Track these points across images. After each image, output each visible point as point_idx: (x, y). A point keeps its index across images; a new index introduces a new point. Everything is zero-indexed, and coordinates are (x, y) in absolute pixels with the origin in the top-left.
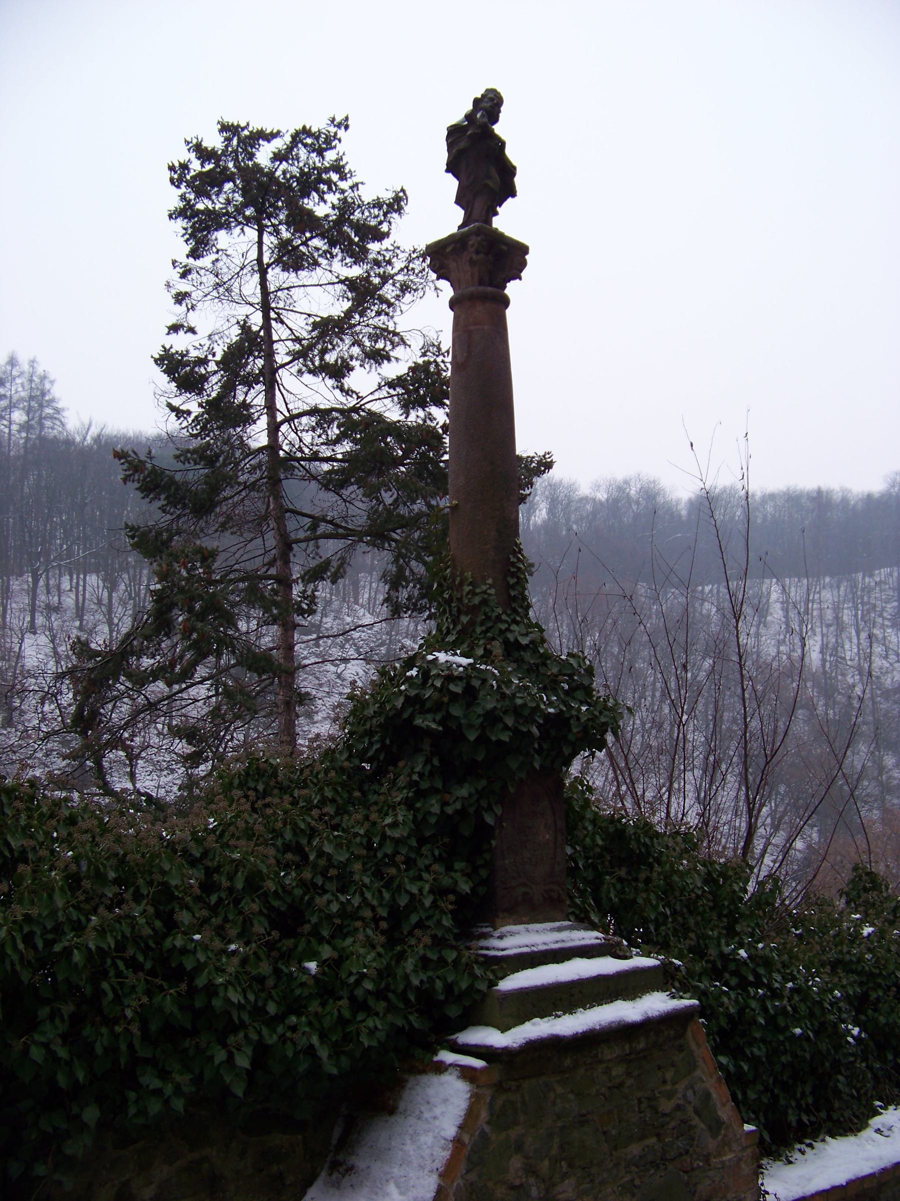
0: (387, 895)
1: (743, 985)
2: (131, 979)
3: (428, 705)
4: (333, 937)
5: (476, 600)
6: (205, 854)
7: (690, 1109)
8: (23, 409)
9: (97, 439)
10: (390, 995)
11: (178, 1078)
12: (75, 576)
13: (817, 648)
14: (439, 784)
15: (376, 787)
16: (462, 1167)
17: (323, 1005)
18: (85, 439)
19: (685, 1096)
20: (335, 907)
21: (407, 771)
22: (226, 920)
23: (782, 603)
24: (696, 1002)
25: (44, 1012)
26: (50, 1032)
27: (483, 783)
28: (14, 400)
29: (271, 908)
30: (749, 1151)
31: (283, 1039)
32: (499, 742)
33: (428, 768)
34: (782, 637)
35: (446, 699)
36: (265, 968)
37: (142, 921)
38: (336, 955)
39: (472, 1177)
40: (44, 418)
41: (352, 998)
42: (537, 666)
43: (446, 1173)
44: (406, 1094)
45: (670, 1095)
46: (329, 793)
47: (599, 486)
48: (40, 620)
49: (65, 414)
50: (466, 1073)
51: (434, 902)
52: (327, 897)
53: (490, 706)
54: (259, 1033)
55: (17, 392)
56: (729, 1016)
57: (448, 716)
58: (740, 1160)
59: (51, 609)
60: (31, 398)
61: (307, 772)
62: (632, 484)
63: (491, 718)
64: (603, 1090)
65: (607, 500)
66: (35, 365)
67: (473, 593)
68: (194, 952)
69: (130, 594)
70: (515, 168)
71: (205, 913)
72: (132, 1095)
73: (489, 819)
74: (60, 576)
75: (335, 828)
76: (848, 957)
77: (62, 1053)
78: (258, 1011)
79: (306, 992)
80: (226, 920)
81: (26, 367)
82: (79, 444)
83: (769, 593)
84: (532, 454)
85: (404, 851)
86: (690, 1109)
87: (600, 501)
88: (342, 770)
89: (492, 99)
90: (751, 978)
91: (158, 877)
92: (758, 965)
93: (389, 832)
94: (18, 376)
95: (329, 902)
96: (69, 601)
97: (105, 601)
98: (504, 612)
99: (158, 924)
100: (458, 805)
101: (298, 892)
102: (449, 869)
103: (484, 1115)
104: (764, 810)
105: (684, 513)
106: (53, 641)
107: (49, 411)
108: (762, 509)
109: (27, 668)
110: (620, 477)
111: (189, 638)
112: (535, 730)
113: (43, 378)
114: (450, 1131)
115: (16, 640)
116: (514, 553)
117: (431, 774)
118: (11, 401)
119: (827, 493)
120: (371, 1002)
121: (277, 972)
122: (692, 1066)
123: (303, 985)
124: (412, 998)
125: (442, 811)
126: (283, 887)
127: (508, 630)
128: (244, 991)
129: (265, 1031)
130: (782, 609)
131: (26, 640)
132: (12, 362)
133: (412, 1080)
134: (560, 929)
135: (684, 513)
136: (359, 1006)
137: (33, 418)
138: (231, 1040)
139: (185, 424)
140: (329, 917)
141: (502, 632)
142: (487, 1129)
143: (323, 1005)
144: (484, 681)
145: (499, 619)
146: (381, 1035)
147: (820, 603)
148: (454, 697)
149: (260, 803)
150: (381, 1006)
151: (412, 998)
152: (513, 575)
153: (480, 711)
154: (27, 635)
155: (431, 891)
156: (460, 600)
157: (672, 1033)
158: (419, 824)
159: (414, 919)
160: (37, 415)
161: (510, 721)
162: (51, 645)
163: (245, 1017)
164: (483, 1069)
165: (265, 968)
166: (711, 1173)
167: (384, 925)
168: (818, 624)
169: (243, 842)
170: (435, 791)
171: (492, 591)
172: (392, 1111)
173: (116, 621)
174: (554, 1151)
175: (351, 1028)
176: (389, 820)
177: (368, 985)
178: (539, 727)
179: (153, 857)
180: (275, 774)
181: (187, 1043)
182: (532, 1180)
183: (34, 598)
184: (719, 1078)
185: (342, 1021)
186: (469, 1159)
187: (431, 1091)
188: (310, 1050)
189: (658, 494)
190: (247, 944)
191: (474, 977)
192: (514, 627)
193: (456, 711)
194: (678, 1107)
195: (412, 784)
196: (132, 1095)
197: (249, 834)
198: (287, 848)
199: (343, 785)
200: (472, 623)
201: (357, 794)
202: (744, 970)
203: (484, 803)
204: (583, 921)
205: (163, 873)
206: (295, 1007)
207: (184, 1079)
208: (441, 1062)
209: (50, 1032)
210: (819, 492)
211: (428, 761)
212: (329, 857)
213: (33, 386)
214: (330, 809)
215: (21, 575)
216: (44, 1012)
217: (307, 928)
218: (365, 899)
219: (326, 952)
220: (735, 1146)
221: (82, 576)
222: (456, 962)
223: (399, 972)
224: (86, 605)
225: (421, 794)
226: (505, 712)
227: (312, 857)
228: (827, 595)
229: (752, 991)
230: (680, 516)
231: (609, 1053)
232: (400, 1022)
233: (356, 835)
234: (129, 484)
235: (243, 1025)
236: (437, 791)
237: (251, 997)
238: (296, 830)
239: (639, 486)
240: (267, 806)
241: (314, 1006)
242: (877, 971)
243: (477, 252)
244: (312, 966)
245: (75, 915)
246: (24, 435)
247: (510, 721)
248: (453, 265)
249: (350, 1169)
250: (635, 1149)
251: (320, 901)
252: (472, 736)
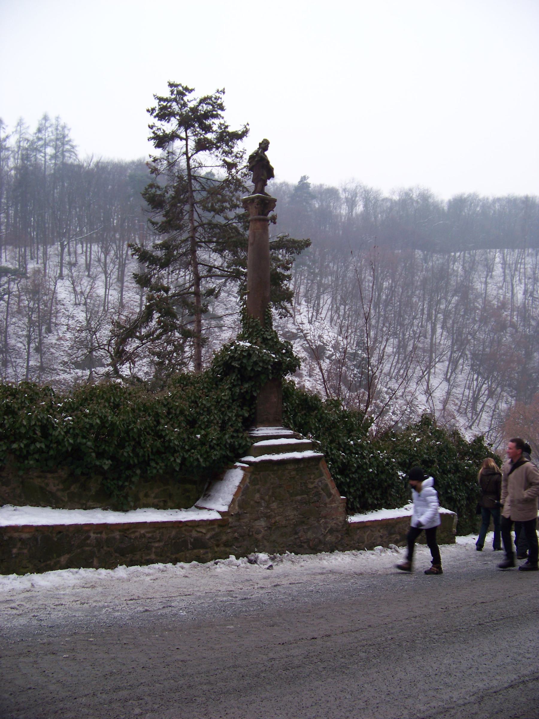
0: (221, 416)
1: (351, 453)
2: (148, 437)
3: (236, 359)
4: (205, 428)
5: (254, 324)
6: (168, 403)
7: (320, 488)
8: (53, 146)
9: (97, 164)
10: (221, 445)
11: (161, 464)
12: (85, 245)
13: (522, 292)
14: (240, 383)
15: (221, 383)
16: (241, 494)
17: (202, 447)
18: (90, 165)
19: (318, 484)
20: (206, 420)
21: (230, 378)
22: (174, 422)
23: (502, 264)
24: (323, 454)
25: (127, 444)
26: (129, 449)
27: (253, 383)
28: (47, 141)
29: (187, 420)
30: (342, 504)
31: (190, 456)
32: (258, 371)
33: (237, 378)
34: (501, 284)
35: (241, 357)
36: (185, 436)
37: (151, 422)
38: (205, 433)
39: (243, 497)
40: (65, 151)
41: (210, 446)
42: (273, 345)
43: (236, 495)
44: (226, 475)
45: (312, 483)
46: (205, 385)
47: (394, 192)
48: (65, 272)
49: (77, 149)
50: (243, 468)
51: (236, 419)
52: (203, 417)
53: (255, 359)
54: (183, 454)
55: (48, 136)
56: (343, 463)
57: (242, 362)
58: (338, 507)
59: (72, 265)
60: (57, 139)
61: (199, 378)
62: (414, 191)
63: (255, 363)
64: (288, 478)
65: (399, 200)
66: (59, 120)
67: (253, 321)
68: (165, 431)
69: (117, 256)
70: (273, 169)
71: (168, 420)
72: (148, 468)
73: (255, 394)
74: (76, 245)
75: (207, 396)
76: (405, 448)
77: (131, 455)
78: (183, 448)
79: (197, 443)
80: (174, 422)
81: (53, 121)
82: (86, 168)
83: (495, 258)
84: (302, 239)
85: (227, 403)
86: (320, 488)
87: (395, 200)
88: (210, 378)
89: (265, 144)
90: (354, 451)
91: (155, 410)
92: (358, 447)
93: (223, 398)
94: (50, 127)
95: (204, 418)
96: (82, 260)
97: (103, 260)
98: (263, 328)
99: (155, 423)
100: (245, 390)
101: (195, 415)
102: (242, 409)
103: (248, 480)
104: (484, 386)
105: (446, 208)
106: (73, 284)
107: (67, 147)
108: (492, 207)
109: (58, 299)
110: (406, 186)
111: (160, 325)
112: (270, 367)
113: (64, 127)
114: (237, 484)
115: (52, 283)
116: (267, 308)
117: (238, 380)
118: (45, 142)
119: (533, 198)
120: (216, 447)
121: (189, 438)
122: (321, 475)
123: (196, 441)
124: (228, 446)
125: (240, 392)
126: (191, 413)
127: (264, 334)
128: (179, 442)
129: (185, 454)
130: (502, 268)
131: (58, 284)
132: (46, 118)
133: (228, 471)
134: (278, 429)
135: (446, 208)
136: (212, 448)
137: (58, 152)
138: (176, 455)
139: (156, 227)
140: (204, 422)
141: (262, 335)
142: (248, 484)
143: (202, 447)
144: (254, 351)
145: (261, 330)
146: (218, 456)
147: (525, 264)
148: (244, 356)
149: (184, 388)
150: (218, 448)
151: (228, 446)
152: (267, 315)
153: (252, 361)
154: (59, 281)
155: (235, 416)
156: (249, 323)
157: (314, 463)
158: (233, 395)
159: (230, 424)
160: (61, 149)
161: (261, 364)
162: (72, 286)
163: (179, 449)
164: (248, 467)
165: (185, 436)
166: (327, 509)
167: (220, 425)
168: (523, 278)
169: (179, 400)
170: (238, 385)
171: (259, 321)
172: (222, 480)
173: (109, 272)
174: (270, 493)
175: (209, 454)
176: (223, 394)
177: (214, 442)
178: (271, 366)
179: (153, 404)
180: (189, 379)
181: (163, 455)
182: (263, 501)
183: (62, 259)
184: (332, 480)
185: (207, 452)
186: (243, 492)
187: (233, 474)
188: (197, 460)
189: (429, 197)
190: (180, 429)
191: (247, 441)
192: (266, 333)
193: (245, 361)
194: (315, 487)
195: (231, 383)
196: (148, 468)
197: (181, 398)
198: (192, 402)
199: (210, 383)
200: (252, 331)
201: (214, 386)
202: (351, 448)
203: (253, 389)
204: (287, 427)
205: (156, 408)
206: (194, 448)
207: (162, 464)
208: (236, 466)
209: (129, 449)
210: (527, 198)
211: (237, 376)
212: (205, 405)
213: (58, 132)
214: (206, 390)
215: (53, 244)
216: (127, 444)
217: (197, 425)
218: (215, 417)
219: (203, 432)
220: (337, 502)
221: (89, 245)
222: (242, 437)
223: (224, 439)
224: (92, 262)
225: (234, 386)
226: (260, 361)
227: (199, 405)
228: (529, 260)
229: (353, 455)
230: (443, 209)
231: (290, 467)
232: (224, 453)
233: (213, 398)
234: (134, 256)
235: (178, 451)
236: (239, 385)
237: (181, 443)
238: (195, 396)
239: (418, 192)
240: (186, 389)
241: (199, 447)
242: (416, 454)
243: (257, 205)
244: (199, 436)
245: (134, 419)
246: (53, 161)
247: (261, 364)
248: (250, 207)
249: (209, 495)
250: (299, 498)
251: (202, 418)
252: (249, 369)
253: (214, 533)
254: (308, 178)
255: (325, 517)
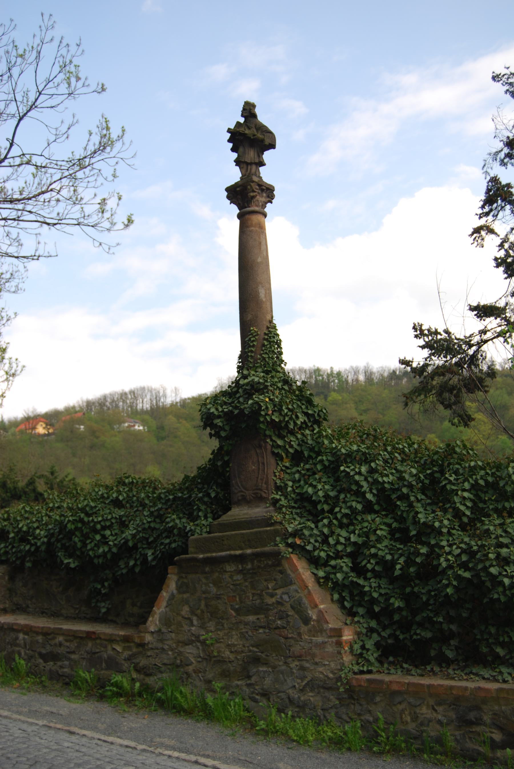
19: (281, 598)
39: (167, 609)
45: (272, 596)
157: (270, 563)
186: (167, 603)
194: (278, 603)
250: (251, 618)
253: (130, 653)
254: (229, 129)
255: (299, 657)
